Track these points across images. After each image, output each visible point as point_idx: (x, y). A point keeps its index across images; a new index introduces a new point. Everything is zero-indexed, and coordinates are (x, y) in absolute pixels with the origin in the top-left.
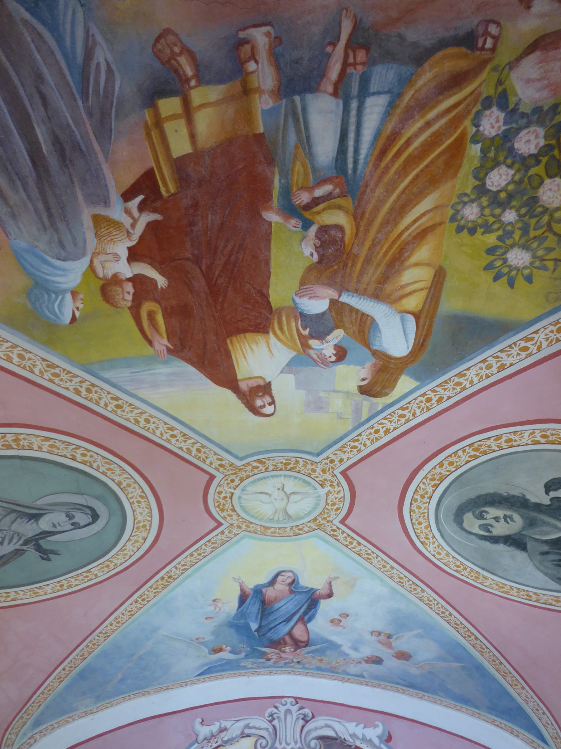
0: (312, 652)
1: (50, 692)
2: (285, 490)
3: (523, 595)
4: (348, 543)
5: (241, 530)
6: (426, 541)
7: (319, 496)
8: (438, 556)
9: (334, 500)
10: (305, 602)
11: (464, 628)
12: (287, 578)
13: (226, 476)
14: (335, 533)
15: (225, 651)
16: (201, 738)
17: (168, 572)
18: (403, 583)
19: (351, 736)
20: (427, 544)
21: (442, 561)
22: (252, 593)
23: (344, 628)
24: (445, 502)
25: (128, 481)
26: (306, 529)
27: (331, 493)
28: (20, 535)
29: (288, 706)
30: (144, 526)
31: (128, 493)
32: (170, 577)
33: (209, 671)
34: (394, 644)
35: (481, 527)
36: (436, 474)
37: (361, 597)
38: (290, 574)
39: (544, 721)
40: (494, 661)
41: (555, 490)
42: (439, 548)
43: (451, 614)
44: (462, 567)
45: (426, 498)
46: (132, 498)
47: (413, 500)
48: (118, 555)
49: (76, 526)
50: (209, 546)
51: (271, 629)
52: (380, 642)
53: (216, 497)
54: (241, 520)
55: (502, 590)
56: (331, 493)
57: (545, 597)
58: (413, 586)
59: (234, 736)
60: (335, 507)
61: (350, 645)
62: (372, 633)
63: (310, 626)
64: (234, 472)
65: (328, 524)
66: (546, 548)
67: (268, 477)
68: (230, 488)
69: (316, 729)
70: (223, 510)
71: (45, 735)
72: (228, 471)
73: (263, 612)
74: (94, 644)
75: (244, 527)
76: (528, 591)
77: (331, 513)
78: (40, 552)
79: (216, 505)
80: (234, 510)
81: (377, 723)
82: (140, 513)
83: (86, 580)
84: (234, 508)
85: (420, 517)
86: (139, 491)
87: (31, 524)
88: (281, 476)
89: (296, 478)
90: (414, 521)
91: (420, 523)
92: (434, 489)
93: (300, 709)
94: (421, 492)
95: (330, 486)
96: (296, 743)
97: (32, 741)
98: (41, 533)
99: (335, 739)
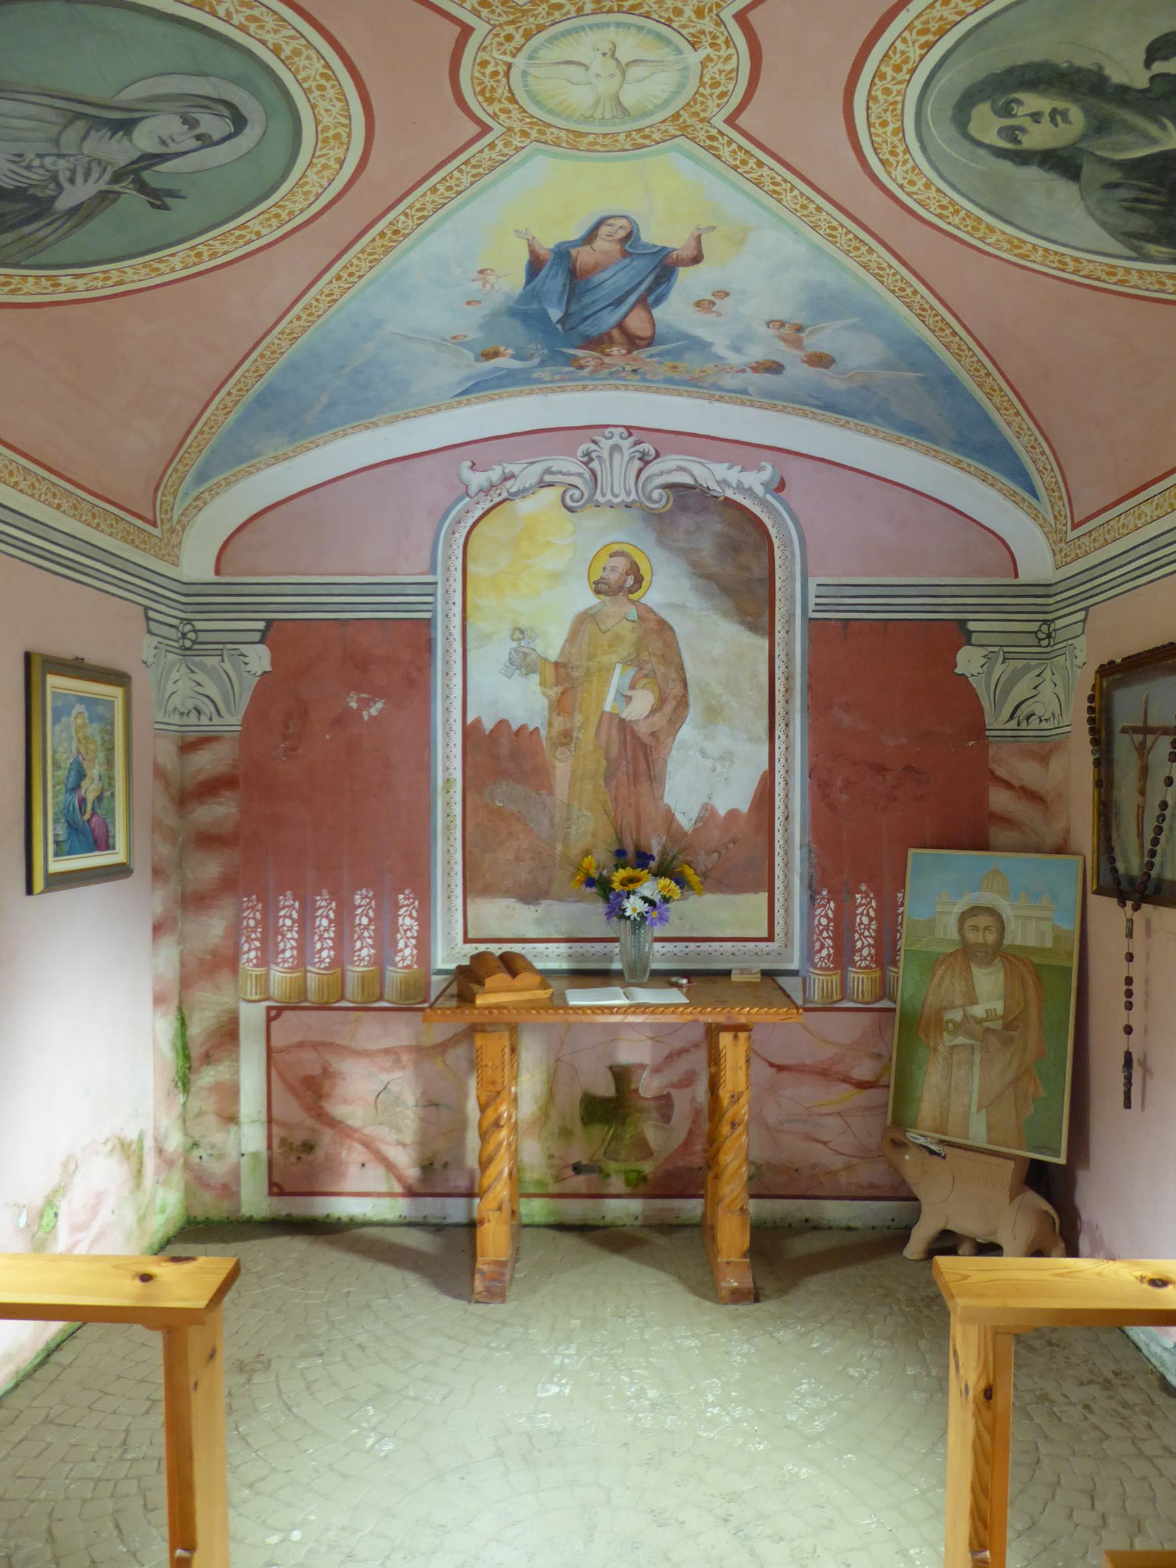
0: (659, 354)
1: (214, 430)
2: (617, 55)
3: (1053, 262)
4: (738, 163)
5: (528, 141)
6: (891, 159)
7: (686, 69)
8: (909, 189)
9: (717, 76)
10: (650, 272)
11: (935, 316)
12: (618, 229)
13: (494, 26)
14: (715, 144)
15: (504, 355)
16: (473, 489)
17: (391, 223)
18: (835, 237)
19: (718, 483)
20: (891, 164)
21: (915, 197)
22: (551, 257)
23: (719, 315)
24: (942, 80)
25: (294, 43)
26: (657, 136)
27: (711, 60)
28: (104, 164)
29: (616, 440)
30: (337, 136)
31: (297, 70)
32: (396, 232)
33: (476, 389)
34: (806, 342)
35: (1002, 131)
36: (933, 19)
37: (758, 259)
38: (624, 222)
39: (1040, 464)
40: (977, 370)
41: (1166, 58)
42: (914, 173)
43: (915, 292)
44: (951, 209)
45: (905, 71)
46: (306, 79)
47: (879, 75)
48: (293, 195)
49: (205, 141)
50: (468, 173)
51: (587, 318)
52: (782, 339)
53: (477, 74)
54: (528, 120)
55: (1016, 251)
56: (711, 60)
57: (1091, 267)
58: (854, 243)
59: (527, 485)
60: (717, 91)
61: (728, 342)
62: (768, 324)
63: (657, 312)
64: (511, 17)
65: (701, 126)
66: (1115, 176)
67: (583, 28)
68: (504, 53)
69: (662, 473)
70: (491, 101)
71: (218, 493)
72: (500, 15)
73: (572, 289)
74: (273, 352)
75: (534, 134)
76: (1063, 255)
77: (710, 103)
78: (147, 195)
79: (478, 89)
80: (513, 99)
81: (763, 464)
82: (327, 111)
83: (241, 242)
84: (513, 95)
85: (886, 111)
86: (319, 65)
87: (119, 141)
88: (608, 25)
89: (640, 28)
90: (872, 120)
91: (884, 124)
92: (923, 52)
93: (635, 444)
94: (896, 59)
95: (712, 45)
96: (628, 493)
97: (200, 503)
98: (140, 159)
99: (693, 488)
